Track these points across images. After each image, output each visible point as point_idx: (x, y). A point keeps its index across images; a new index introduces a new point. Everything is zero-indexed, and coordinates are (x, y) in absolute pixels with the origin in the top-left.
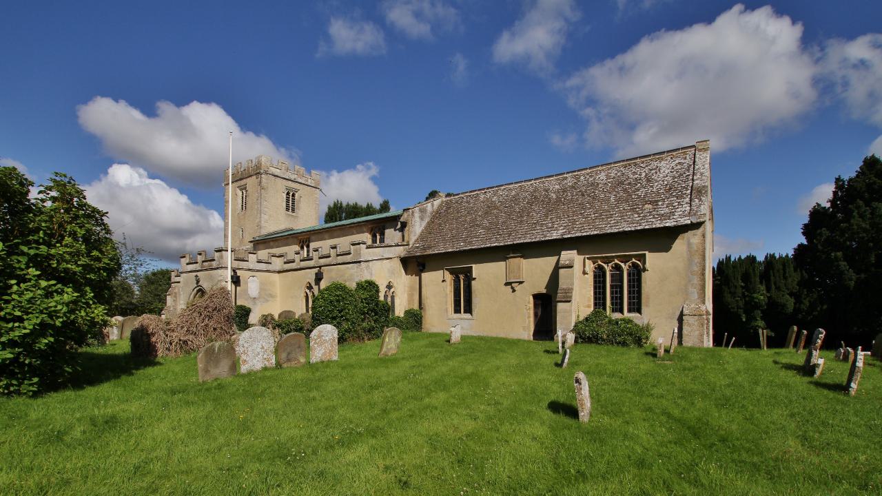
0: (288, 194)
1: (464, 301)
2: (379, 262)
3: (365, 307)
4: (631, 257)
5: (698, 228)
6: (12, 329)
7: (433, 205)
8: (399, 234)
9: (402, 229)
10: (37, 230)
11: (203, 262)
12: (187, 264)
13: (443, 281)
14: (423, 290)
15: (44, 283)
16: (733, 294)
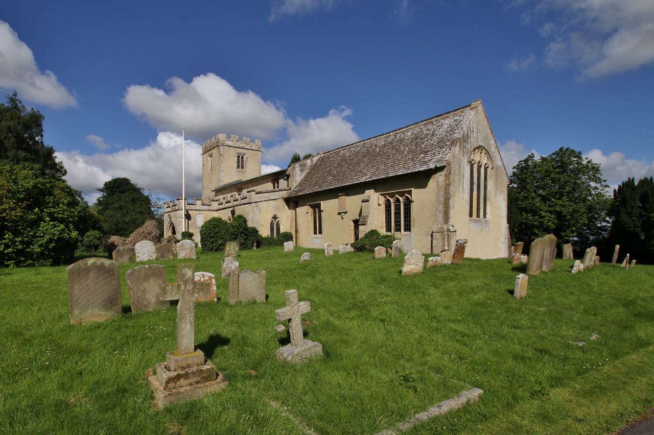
0: (238, 157)
1: (318, 228)
2: (267, 202)
3: (236, 231)
4: (404, 192)
5: (442, 171)
6: (40, 240)
7: (312, 161)
8: (286, 182)
9: (287, 180)
10: (50, 202)
11: (173, 206)
12: (167, 208)
13: (307, 213)
14: (297, 219)
15: (51, 223)
16: (630, 214)
